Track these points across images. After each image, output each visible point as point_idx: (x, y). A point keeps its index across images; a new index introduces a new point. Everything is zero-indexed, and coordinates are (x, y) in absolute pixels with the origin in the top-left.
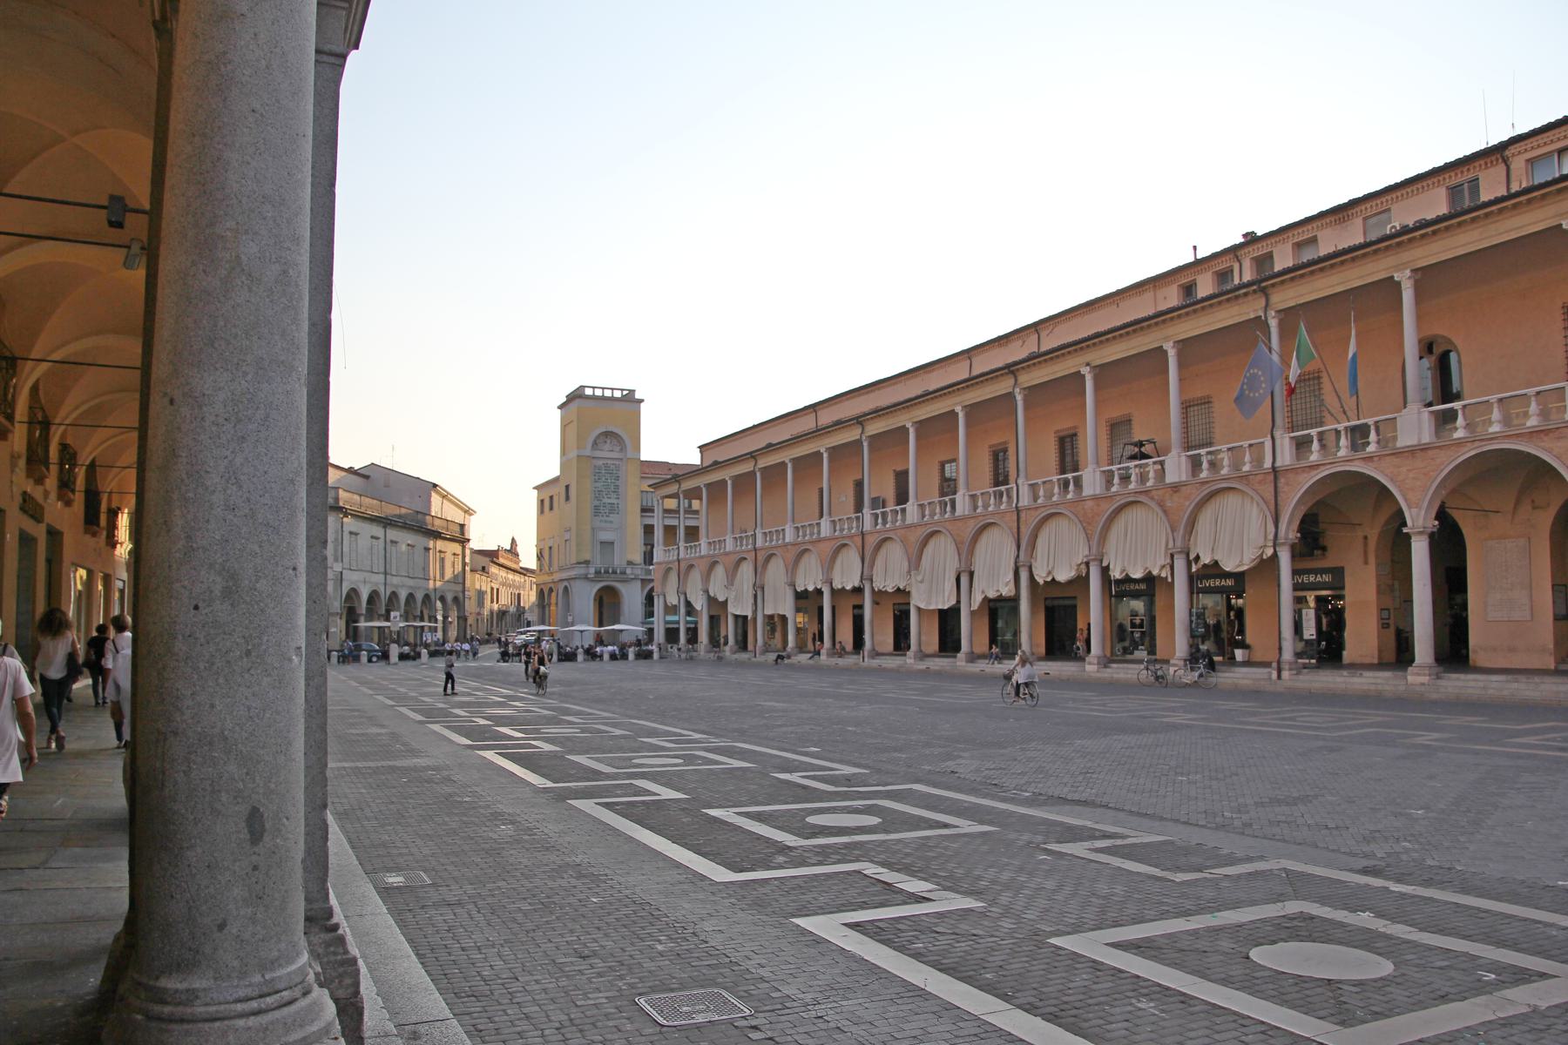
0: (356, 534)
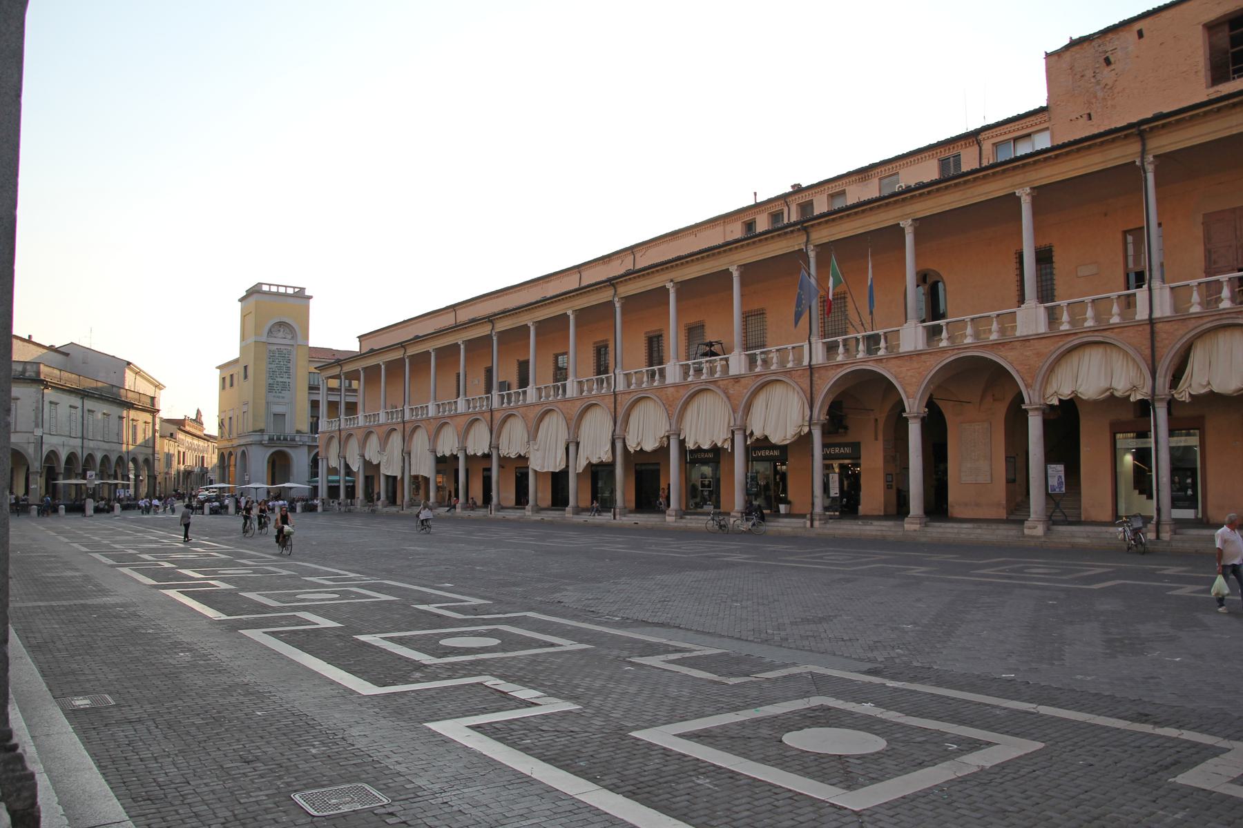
0: (57, 404)
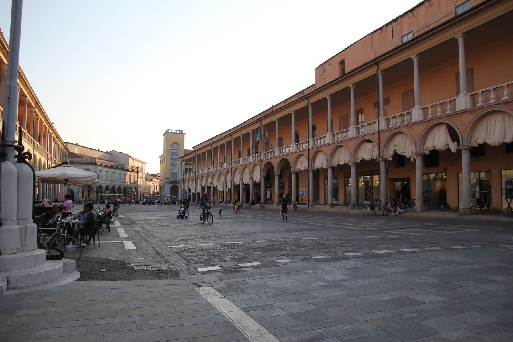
0: (102, 171)
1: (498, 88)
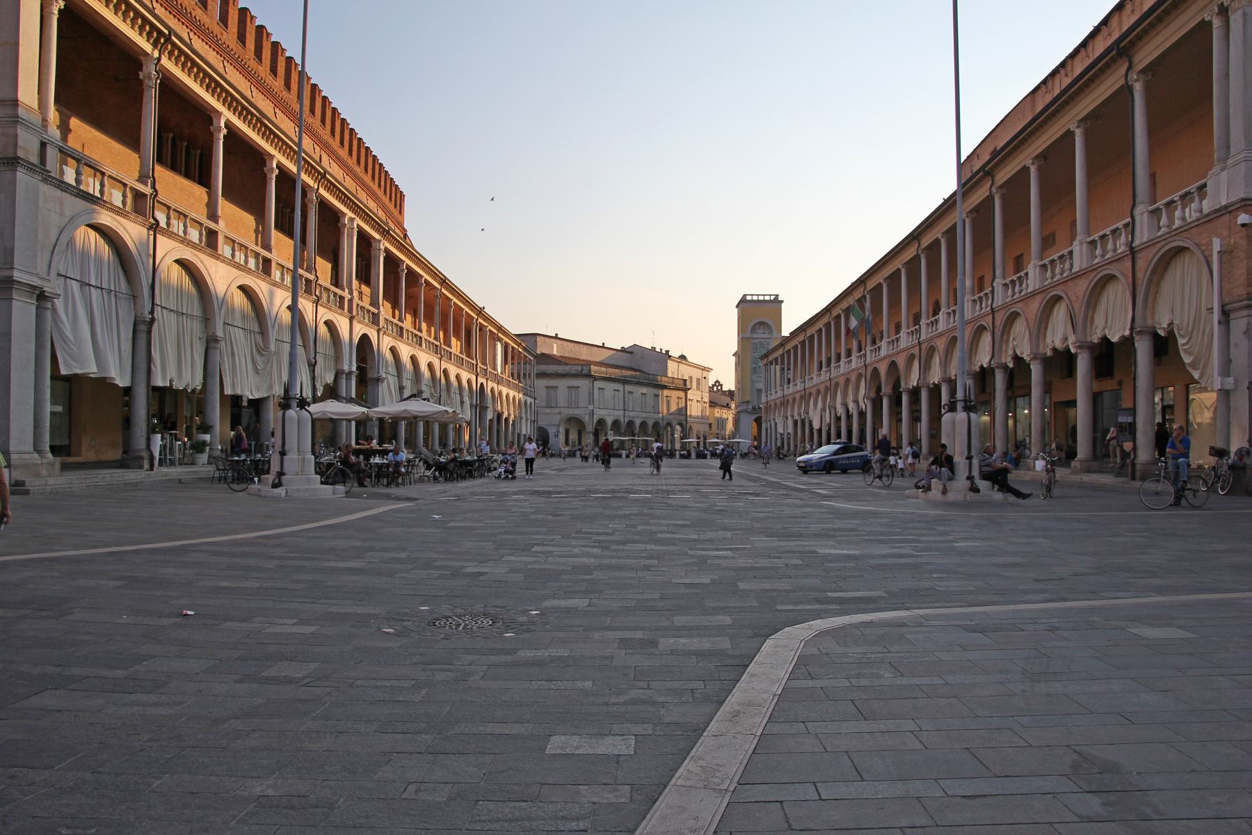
0: (603, 389)
1: (593, 348)
